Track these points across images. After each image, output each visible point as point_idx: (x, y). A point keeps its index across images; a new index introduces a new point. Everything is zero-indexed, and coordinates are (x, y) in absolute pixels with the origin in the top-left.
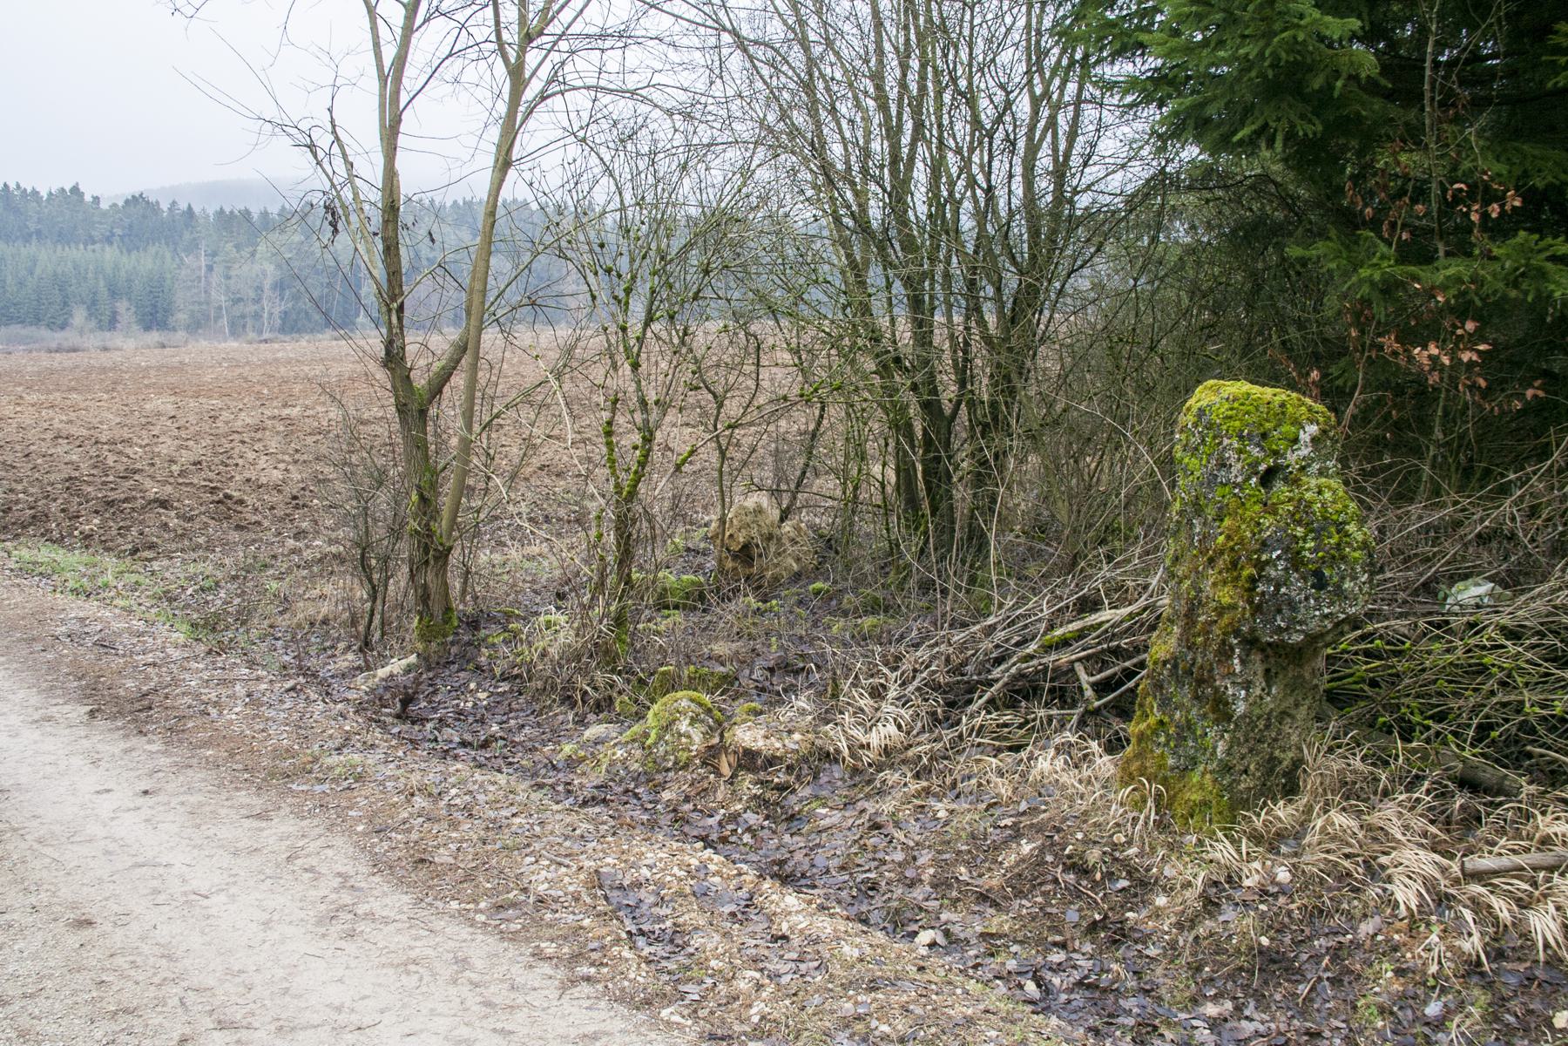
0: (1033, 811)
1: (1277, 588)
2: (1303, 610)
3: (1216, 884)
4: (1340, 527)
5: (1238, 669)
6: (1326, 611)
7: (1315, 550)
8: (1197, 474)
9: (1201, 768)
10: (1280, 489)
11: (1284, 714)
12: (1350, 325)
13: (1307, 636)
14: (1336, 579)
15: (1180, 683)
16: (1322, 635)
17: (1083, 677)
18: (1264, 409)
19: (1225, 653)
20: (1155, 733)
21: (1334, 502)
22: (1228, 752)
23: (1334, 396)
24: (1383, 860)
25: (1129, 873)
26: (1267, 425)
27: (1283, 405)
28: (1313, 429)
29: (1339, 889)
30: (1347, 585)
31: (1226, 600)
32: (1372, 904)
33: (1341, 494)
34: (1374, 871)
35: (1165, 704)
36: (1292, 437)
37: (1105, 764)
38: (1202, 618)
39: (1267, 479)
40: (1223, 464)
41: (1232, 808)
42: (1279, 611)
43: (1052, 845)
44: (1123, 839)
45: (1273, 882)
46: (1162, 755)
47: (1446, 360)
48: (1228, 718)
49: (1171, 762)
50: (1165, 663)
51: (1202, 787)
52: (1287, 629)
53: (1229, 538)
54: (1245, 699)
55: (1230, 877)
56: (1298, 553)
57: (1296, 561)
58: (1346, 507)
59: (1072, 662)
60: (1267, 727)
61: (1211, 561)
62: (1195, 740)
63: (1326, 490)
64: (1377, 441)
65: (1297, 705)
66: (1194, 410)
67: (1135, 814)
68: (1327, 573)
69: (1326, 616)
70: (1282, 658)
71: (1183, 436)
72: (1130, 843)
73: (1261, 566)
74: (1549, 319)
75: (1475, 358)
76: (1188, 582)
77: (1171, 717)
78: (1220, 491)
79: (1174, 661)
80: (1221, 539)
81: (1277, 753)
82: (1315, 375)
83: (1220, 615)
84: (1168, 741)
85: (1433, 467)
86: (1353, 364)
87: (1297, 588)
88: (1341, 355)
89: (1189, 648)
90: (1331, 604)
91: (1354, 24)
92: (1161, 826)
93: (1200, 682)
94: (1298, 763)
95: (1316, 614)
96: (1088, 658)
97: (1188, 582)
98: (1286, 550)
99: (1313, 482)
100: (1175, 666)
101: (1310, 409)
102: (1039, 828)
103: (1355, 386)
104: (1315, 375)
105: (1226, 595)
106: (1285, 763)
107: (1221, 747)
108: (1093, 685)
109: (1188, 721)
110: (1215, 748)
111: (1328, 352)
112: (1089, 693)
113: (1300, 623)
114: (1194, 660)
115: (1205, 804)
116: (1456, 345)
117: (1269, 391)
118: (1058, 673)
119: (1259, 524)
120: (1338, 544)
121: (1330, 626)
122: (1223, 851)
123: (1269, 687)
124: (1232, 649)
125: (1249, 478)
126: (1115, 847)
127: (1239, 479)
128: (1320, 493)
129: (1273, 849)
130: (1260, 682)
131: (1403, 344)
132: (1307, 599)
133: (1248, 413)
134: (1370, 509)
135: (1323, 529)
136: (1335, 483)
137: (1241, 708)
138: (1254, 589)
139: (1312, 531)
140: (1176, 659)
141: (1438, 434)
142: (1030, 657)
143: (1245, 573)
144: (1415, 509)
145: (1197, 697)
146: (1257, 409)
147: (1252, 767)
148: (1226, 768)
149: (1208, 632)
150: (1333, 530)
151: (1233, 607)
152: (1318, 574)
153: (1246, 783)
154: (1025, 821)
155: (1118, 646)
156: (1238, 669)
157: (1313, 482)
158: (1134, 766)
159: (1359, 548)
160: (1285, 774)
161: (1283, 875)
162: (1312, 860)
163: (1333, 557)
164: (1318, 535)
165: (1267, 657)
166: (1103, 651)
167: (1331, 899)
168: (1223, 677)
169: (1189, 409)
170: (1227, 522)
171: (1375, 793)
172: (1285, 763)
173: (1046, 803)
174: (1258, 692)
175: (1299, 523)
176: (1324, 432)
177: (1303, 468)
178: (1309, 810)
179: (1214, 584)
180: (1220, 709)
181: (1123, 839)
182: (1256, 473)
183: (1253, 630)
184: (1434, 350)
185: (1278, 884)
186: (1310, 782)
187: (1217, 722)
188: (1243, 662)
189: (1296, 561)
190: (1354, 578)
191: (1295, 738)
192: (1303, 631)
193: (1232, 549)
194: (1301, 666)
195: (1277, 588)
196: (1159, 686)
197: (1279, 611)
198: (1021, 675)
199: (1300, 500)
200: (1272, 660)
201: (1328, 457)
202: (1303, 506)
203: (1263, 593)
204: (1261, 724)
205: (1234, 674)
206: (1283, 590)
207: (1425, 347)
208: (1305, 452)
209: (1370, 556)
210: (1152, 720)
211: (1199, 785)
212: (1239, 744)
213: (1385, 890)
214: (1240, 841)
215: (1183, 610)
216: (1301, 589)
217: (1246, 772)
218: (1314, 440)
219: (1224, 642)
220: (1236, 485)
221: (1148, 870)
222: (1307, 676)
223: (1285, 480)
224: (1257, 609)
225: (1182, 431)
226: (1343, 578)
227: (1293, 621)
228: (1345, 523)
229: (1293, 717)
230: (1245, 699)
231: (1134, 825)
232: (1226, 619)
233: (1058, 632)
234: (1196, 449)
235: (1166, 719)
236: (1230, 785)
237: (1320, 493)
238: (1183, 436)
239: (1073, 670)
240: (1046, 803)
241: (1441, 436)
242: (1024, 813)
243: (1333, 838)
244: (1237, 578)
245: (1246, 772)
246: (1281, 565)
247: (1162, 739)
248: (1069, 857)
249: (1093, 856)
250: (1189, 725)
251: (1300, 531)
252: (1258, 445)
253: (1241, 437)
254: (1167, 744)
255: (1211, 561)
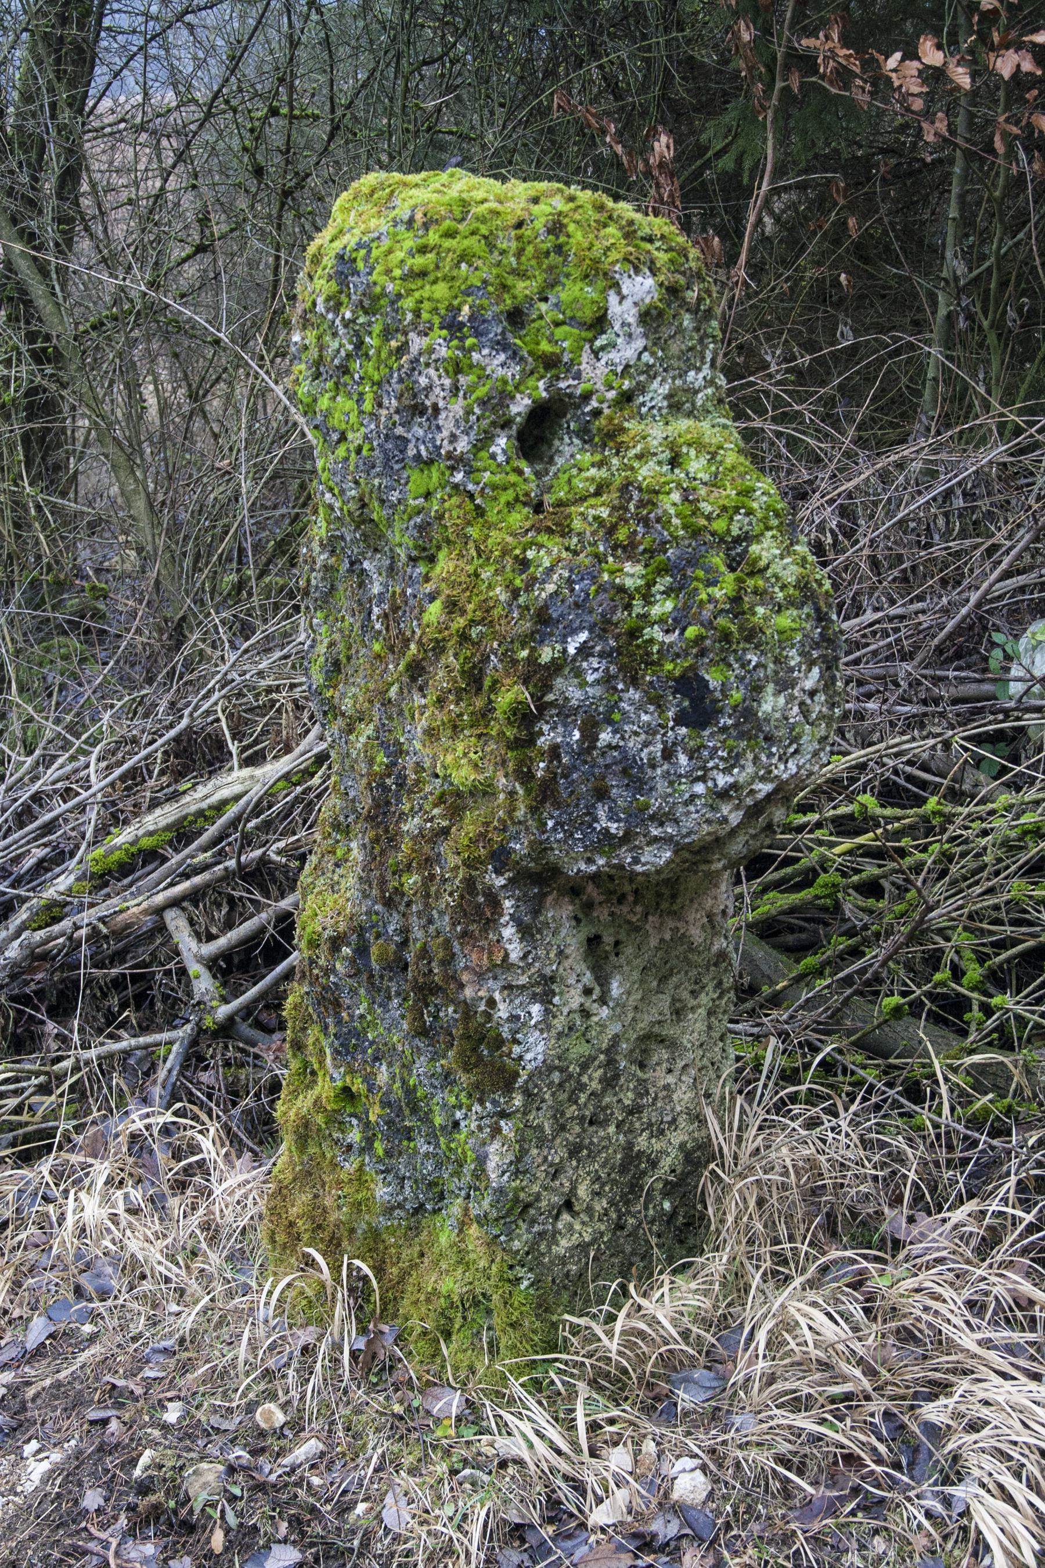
0: (61, 1343)
1: (590, 734)
2: (662, 786)
3: (518, 1532)
4: (736, 550)
5: (515, 951)
6: (723, 780)
7: (677, 622)
8: (355, 438)
9: (456, 1208)
10: (575, 462)
11: (650, 1039)
12: (736, 14)
13: (678, 849)
14: (737, 696)
15: (379, 994)
16: (718, 842)
17: (188, 945)
18: (507, 242)
19: (478, 912)
20: (335, 1120)
21: (714, 483)
22: (517, 1168)
23: (709, 200)
24: (934, 1412)
25: (296, 1523)
26: (523, 288)
27: (556, 227)
28: (642, 287)
29: (832, 1510)
30: (770, 704)
31: (463, 776)
32: (920, 1542)
33: (731, 458)
34: (913, 1450)
35: (349, 1044)
36: (588, 314)
37: (237, 1186)
38: (411, 825)
39: (536, 435)
40: (416, 408)
41: (543, 1307)
42: (602, 794)
43: (103, 1449)
44: (280, 1418)
45: (669, 1506)
46: (360, 1178)
47: (962, 78)
48: (506, 1080)
49: (382, 1192)
50: (336, 944)
51: (462, 1260)
52: (627, 837)
53: (452, 607)
54: (545, 1025)
55: (554, 1503)
56: (634, 633)
57: (630, 657)
58: (747, 493)
59: (159, 911)
60: (610, 1082)
61: (416, 671)
62: (432, 1137)
63: (689, 450)
64: (824, 294)
65: (679, 1012)
66: (329, 261)
67: (306, 1336)
68: (713, 679)
69: (723, 795)
70: (625, 912)
71: (311, 337)
72: (297, 1425)
73: (540, 677)
74: (1039, 73)
75: (1027, 66)
76: (367, 730)
77: (369, 1080)
78: (417, 480)
79: (357, 937)
80: (434, 611)
81: (642, 1142)
82: (663, 145)
83: (455, 812)
84: (369, 1141)
85: (948, 344)
86: (750, 118)
87: (640, 727)
88: (727, 97)
89: (389, 903)
90: (734, 761)
91: (898, 55)
92: (372, 1366)
93: (426, 991)
94: (699, 1156)
95: (696, 795)
96: (194, 897)
97: (367, 730)
98: (603, 627)
99: (656, 433)
100: (362, 951)
101: (629, 233)
102: (70, 1398)
103: (757, 170)
104: (663, 145)
105: (460, 763)
106: (666, 1163)
107: (496, 1156)
108: (212, 964)
109: (409, 1092)
110: (481, 1160)
111: (694, 95)
112: (204, 984)
113: (659, 818)
114: (405, 931)
115: (476, 1302)
116: (984, 38)
117: (519, 190)
118: (117, 943)
119: (524, 564)
120: (736, 600)
121: (735, 819)
122: (528, 1435)
123: (602, 980)
124: (494, 903)
125: (485, 440)
126: (260, 1443)
127: (463, 445)
128: (674, 462)
129: (658, 1405)
130: (576, 973)
131: (860, 51)
132: (668, 754)
133: (464, 257)
134: (815, 460)
135: (693, 562)
136: (717, 430)
137: (534, 1050)
138: (531, 741)
139: (663, 570)
140: (361, 930)
141: (955, 265)
142: (53, 912)
143: (504, 699)
144: (916, 452)
145: (422, 1032)
146: (489, 241)
147: (583, 1191)
148: (517, 1209)
149: (428, 862)
150: (717, 560)
151: (484, 791)
152: (689, 684)
153: (573, 1233)
154: (42, 1377)
155: (264, 860)
156: (515, 951)
157: (656, 433)
158: (300, 1203)
159: (791, 603)
160: (669, 1189)
161: (689, 1484)
162: (759, 1432)
163: (726, 636)
164: (681, 577)
165: (589, 906)
166: (228, 876)
167: (816, 1541)
168: (480, 977)
169: (316, 260)
170: (445, 564)
171: (897, 1201)
172: (666, 1163)
173: (94, 1317)
174: (575, 999)
175: (628, 550)
176: (673, 291)
177: (626, 398)
178: (736, 1285)
179: (431, 734)
180: (484, 1058)
181: (280, 1418)
182: (506, 424)
183: (540, 849)
184: (932, 55)
185: (679, 1510)
186: (732, 1205)
187: (478, 1093)
188: (526, 932)
189: (630, 657)
190: (784, 685)
191: (683, 1096)
192: (668, 840)
193: (464, 637)
194: (677, 915)
195: (590, 734)
196: (329, 1001)
197: (602, 794)
198: (37, 957)
199: (625, 489)
200: (602, 913)
201: (689, 360)
202: (635, 503)
203: (554, 752)
204: (593, 1079)
205: (506, 964)
206: (605, 737)
207: (911, 54)
208: (627, 352)
209: (821, 617)
210: (324, 1089)
211: (454, 1259)
212: (542, 1142)
213: (947, 1501)
214: (572, 1393)
215: (366, 803)
216: (650, 731)
217: (568, 1205)
218: (649, 317)
219: (470, 884)
220: (456, 462)
221: (344, 1509)
222: (697, 934)
223: (584, 433)
224: (545, 794)
225: (306, 323)
226: (757, 689)
227: (638, 816)
228: (746, 538)
229: (672, 1044)
230: (545, 1025)
231: (305, 1372)
232: (469, 826)
233: (122, 837)
234: (344, 370)
235: (358, 1085)
236: (532, 1248)
237: (674, 462)
238: (311, 337)
239: (161, 928)
240: (94, 1317)
241: (961, 268)
242: (39, 1352)
243: (803, 1366)
244: (485, 714)
245: (568, 1205)
246: (593, 669)
247: (355, 1136)
248: (144, 1488)
249: (204, 1481)
250: (413, 1102)
251: (632, 575)
252: (501, 345)
253: (453, 327)
254: (368, 1147)
255: (416, 671)
